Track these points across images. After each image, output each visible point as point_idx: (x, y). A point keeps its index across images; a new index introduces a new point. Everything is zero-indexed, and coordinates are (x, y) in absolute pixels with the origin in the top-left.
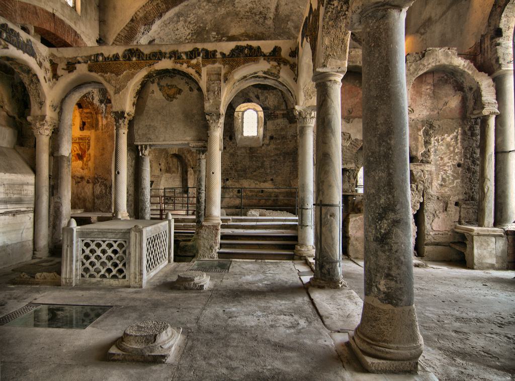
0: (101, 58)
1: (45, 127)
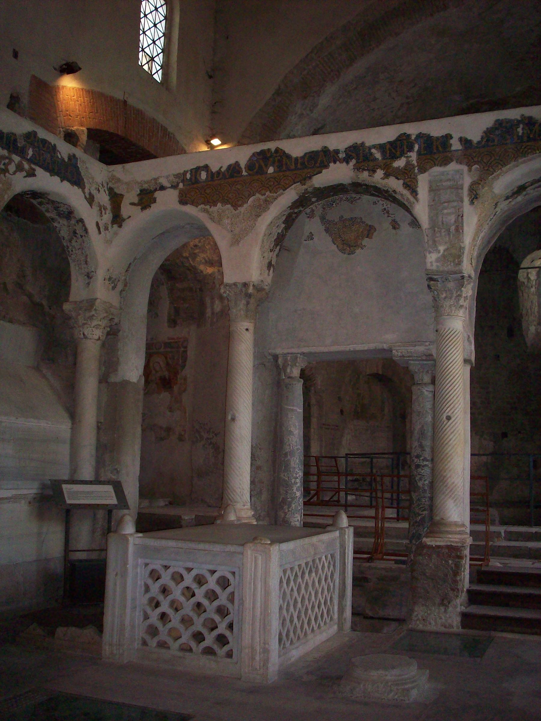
0: (203, 175)
1: (95, 323)
